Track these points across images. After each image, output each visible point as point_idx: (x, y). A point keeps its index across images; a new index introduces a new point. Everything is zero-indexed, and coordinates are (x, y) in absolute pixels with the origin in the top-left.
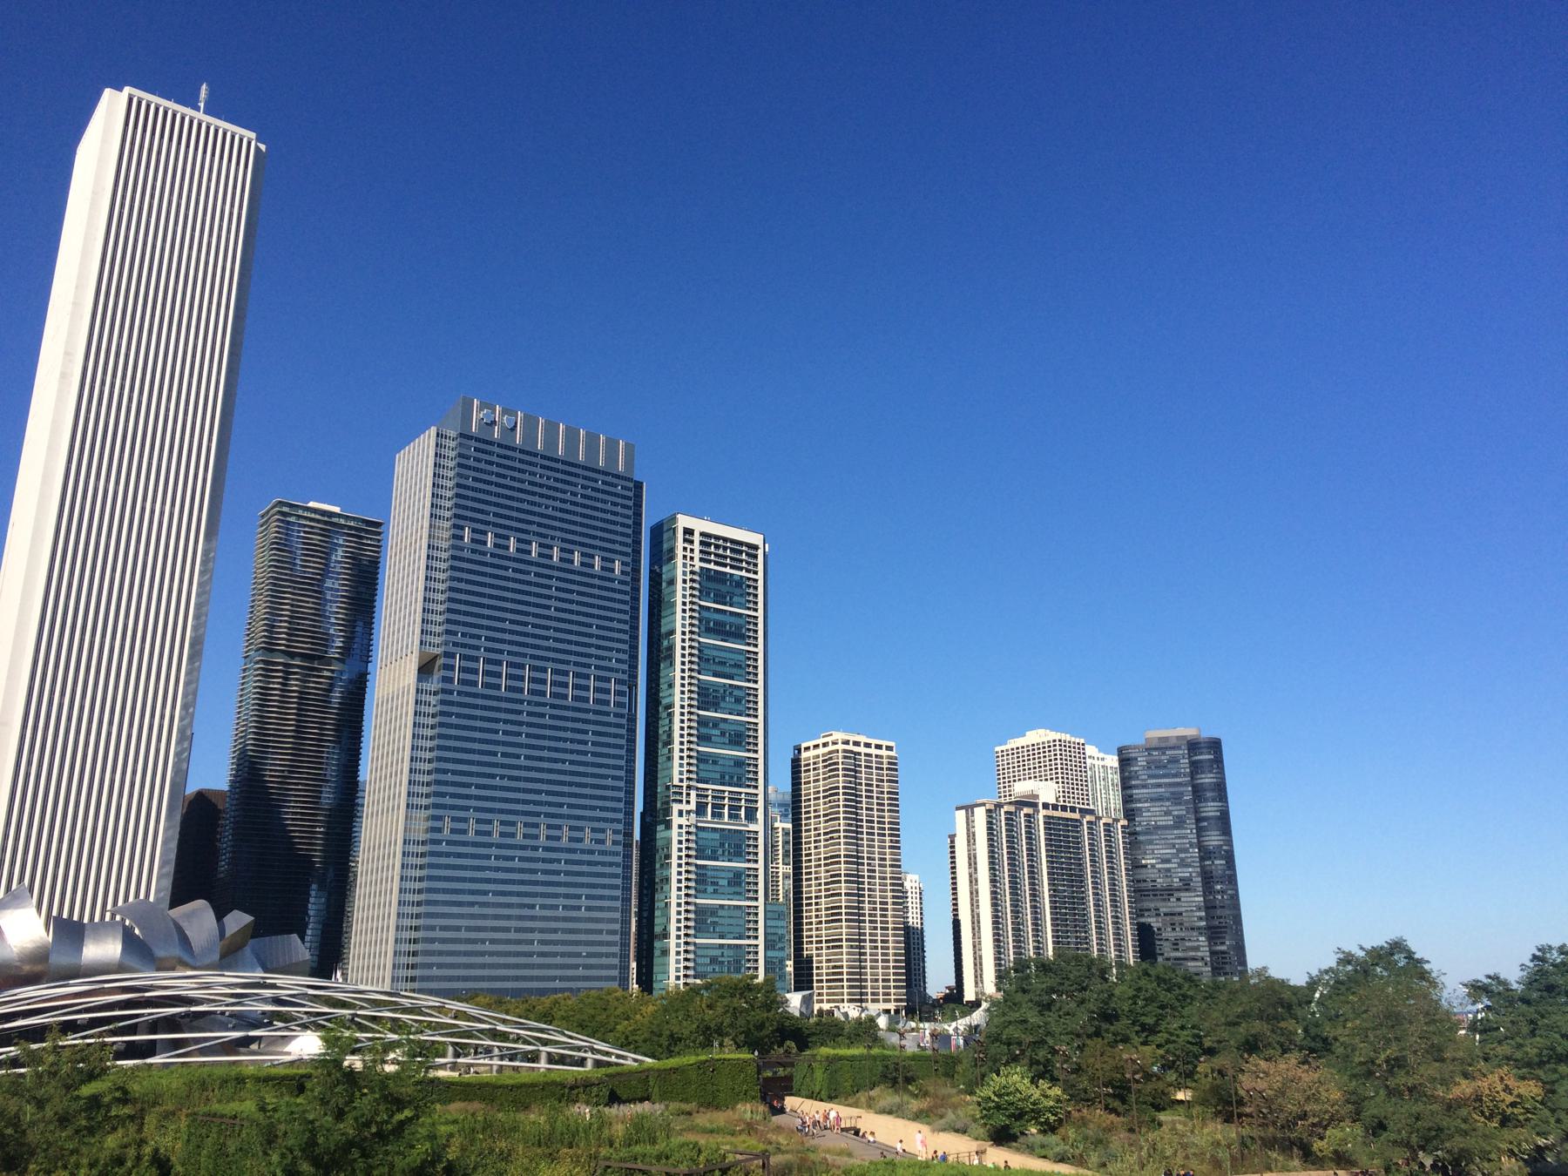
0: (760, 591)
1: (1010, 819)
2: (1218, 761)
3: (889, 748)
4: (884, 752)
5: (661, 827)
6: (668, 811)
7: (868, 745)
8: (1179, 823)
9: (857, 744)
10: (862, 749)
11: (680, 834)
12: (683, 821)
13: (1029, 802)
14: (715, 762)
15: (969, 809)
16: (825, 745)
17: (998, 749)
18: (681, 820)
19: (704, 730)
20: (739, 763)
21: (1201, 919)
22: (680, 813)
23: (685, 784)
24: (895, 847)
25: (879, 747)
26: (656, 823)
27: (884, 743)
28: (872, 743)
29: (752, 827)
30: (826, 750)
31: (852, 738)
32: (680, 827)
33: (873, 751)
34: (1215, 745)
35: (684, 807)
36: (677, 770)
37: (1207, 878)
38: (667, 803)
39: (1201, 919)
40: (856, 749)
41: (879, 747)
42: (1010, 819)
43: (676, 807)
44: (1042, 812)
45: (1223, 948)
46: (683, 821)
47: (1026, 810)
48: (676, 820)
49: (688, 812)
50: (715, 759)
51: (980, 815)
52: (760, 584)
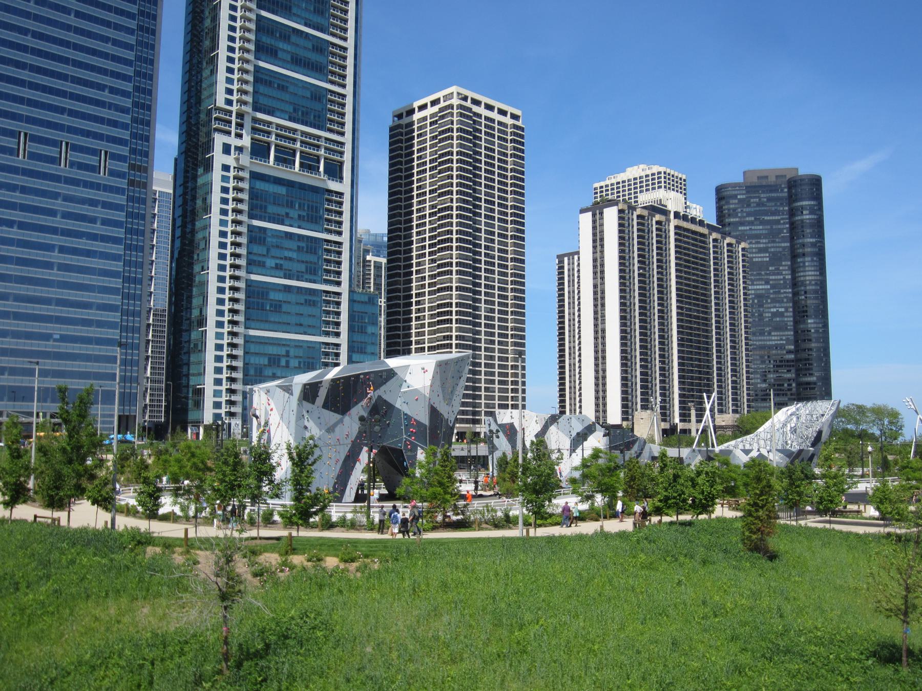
0: (350, 62)
1: (642, 229)
2: (817, 196)
3: (515, 117)
4: (508, 120)
5: (200, 171)
6: (209, 146)
7: (489, 107)
8: (776, 259)
9: (476, 102)
10: (481, 110)
11: (225, 179)
12: (230, 160)
13: (657, 209)
14: (282, 88)
15: (597, 209)
16: (434, 103)
17: (597, 185)
18: (227, 156)
19: (267, 40)
20: (318, 95)
21: (789, 352)
22: (227, 149)
23: (234, 108)
24: (519, 238)
25: (503, 113)
26: (196, 166)
27: (510, 110)
28: (497, 107)
29: (333, 185)
30: (436, 109)
31: (471, 94)
32: (226, 168)
33: (494, 115)
34: (816, 183)
35: (233, 141)
36: (225, 88)
37: (800, 313)
38: (209, 134)
39: (789, 352)
40: (475, 109)
41: (503, 113)
42: (642, 229)
43: (219, 140)
44: (673, 222)
45: (814, 379)
46: (230, 160)
47: (658, 217)
48: (219, 158)
49: (240, 149)
50: (283, 83)
51: (611, 216)
52: (349, 101)
